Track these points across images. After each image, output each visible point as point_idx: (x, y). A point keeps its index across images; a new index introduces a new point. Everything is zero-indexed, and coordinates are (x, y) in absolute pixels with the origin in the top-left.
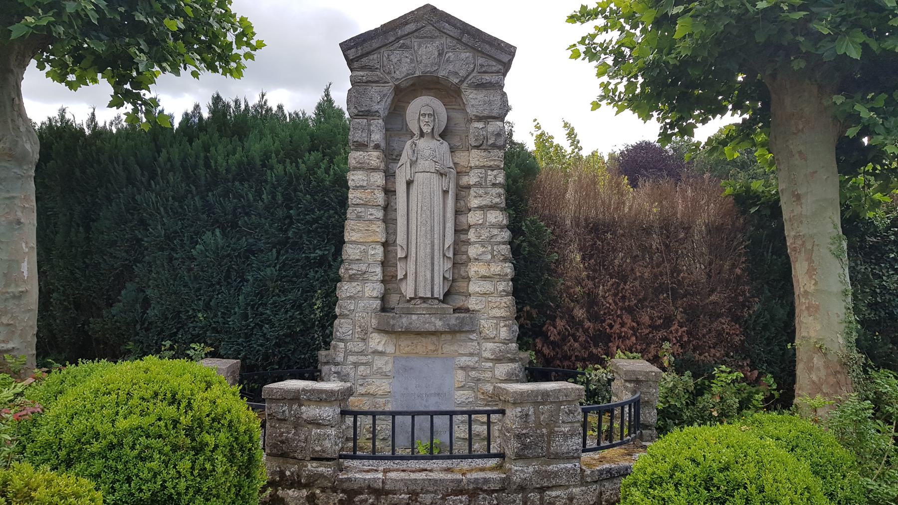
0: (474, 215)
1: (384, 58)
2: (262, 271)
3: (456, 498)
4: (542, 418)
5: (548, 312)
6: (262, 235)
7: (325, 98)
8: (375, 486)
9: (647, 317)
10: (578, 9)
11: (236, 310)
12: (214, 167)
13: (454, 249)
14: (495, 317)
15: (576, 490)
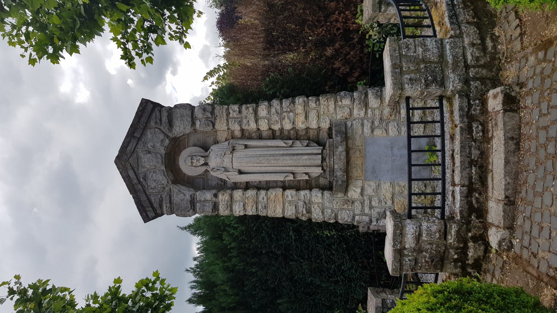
0: (262, 125)
1: (153, 191)
2: (305, 271)
3: (474, 131)
4: (412, 68)
5: (329, 73)
6: (281, 271)
7: (188, 229)
8: (465, 192)
9: (332, 4)
10: (123, 62)
11: (332, 288)
12: (235, 304)
13: (286, 139)
14: (335, 109)
15: (467, 41)
